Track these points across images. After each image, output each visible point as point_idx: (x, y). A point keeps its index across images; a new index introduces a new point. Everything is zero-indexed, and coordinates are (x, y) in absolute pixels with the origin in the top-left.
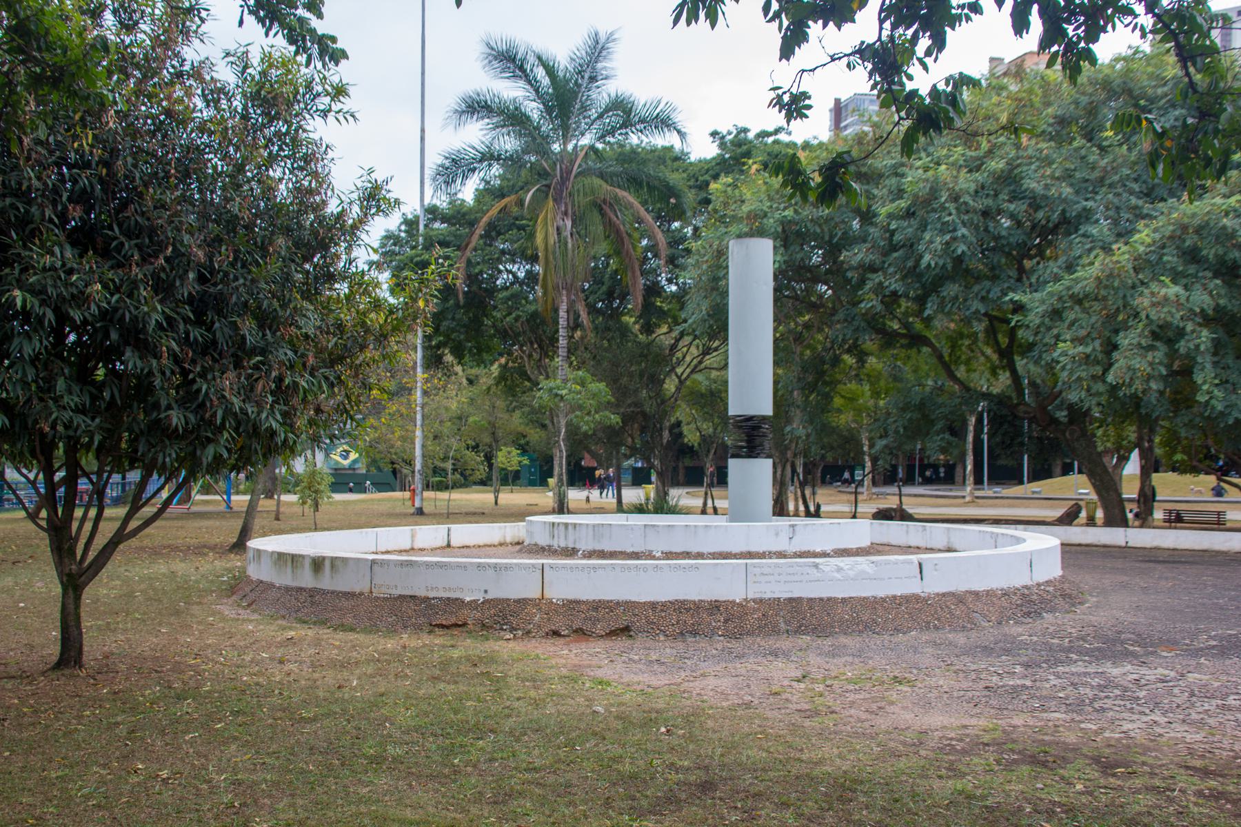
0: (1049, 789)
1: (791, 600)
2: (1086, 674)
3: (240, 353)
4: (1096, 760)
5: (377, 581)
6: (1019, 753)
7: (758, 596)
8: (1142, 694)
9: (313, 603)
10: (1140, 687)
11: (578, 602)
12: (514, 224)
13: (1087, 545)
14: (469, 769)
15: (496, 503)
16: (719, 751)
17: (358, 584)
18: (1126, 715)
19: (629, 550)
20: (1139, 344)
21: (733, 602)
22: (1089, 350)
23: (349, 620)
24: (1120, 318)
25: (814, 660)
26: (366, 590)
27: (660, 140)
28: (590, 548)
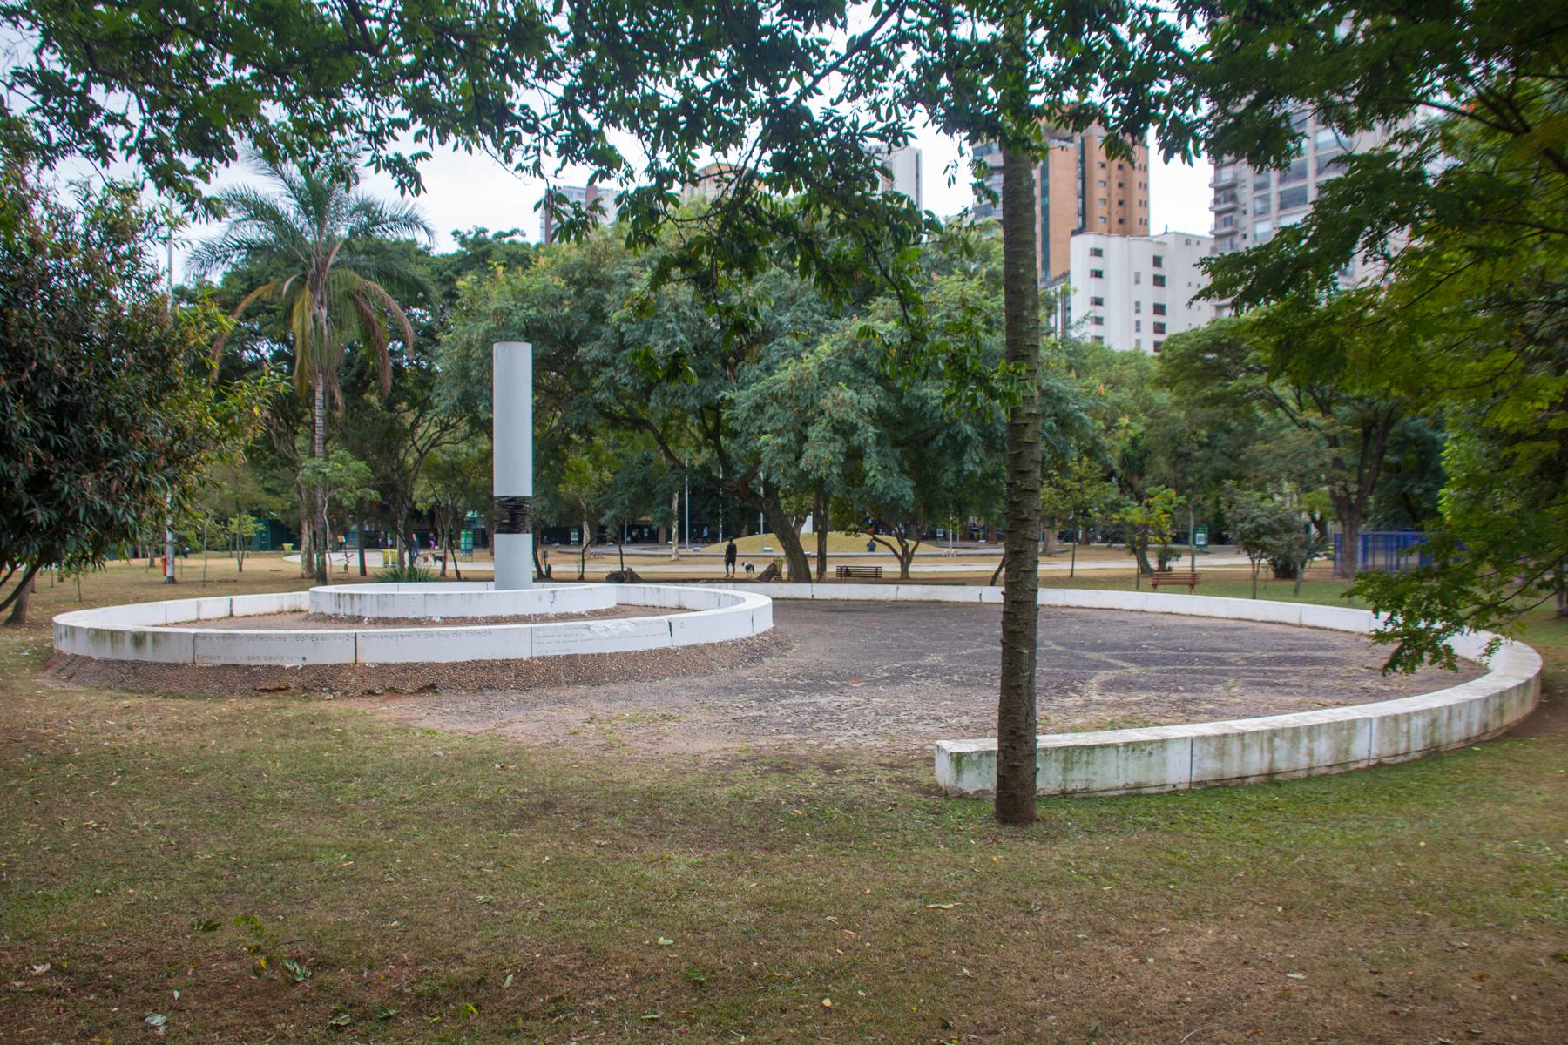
0: (793, 787)
1: (568, 657)
2: (803, 704)
3: (94, 458)
4: (821, 765)
5: (200, 652)
6: (769, 765)
7: (541, 654)
8: (844, 716)
9: (136, 675)
10: (841, 711)
11: (388, 665)
12: (263, 307)
13: (782, 599)
14: (353, 805)
15: (241, 569)
16: (548, 779)
17: (182, 656)
18: (836, 732)
19: (411, 616)
20: (824, 437)
21: (521, 660)
22: (785, 441)
23: (175, 688)
24: (809, 414)
25: (597, 706)
26: (189, 660)
27: (405, 235)
28: (375, 615)
